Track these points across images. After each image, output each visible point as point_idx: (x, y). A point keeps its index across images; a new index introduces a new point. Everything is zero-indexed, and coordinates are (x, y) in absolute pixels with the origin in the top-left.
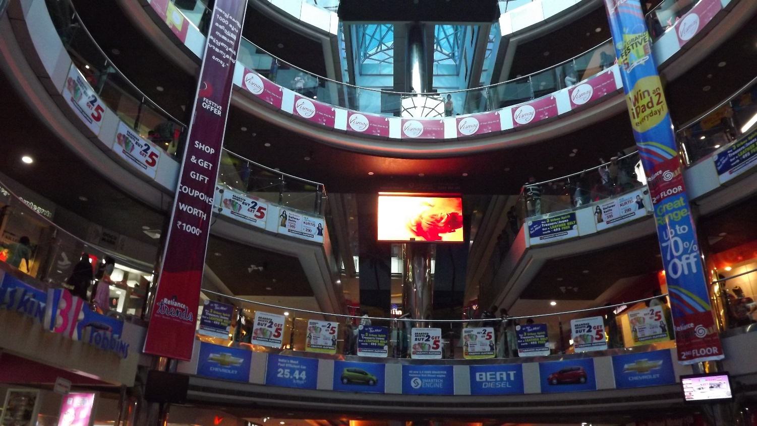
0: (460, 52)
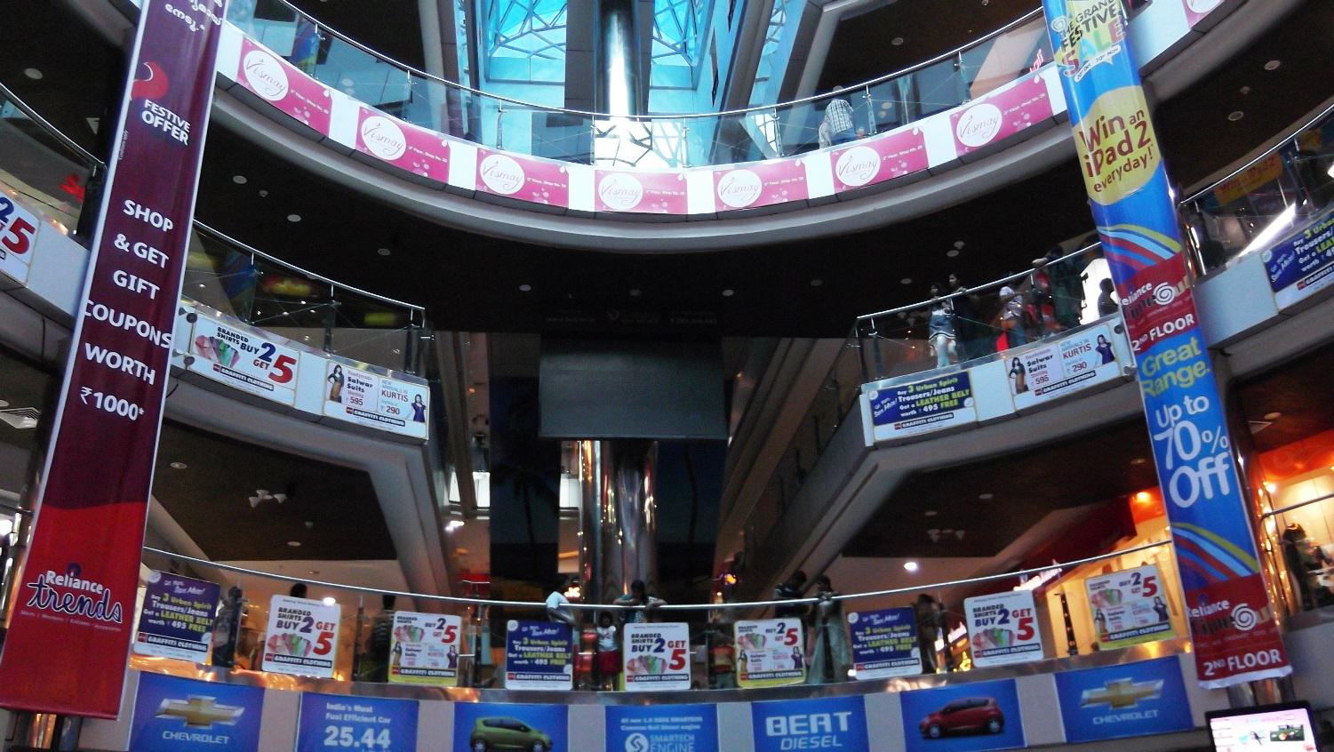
0: (700, 42)
